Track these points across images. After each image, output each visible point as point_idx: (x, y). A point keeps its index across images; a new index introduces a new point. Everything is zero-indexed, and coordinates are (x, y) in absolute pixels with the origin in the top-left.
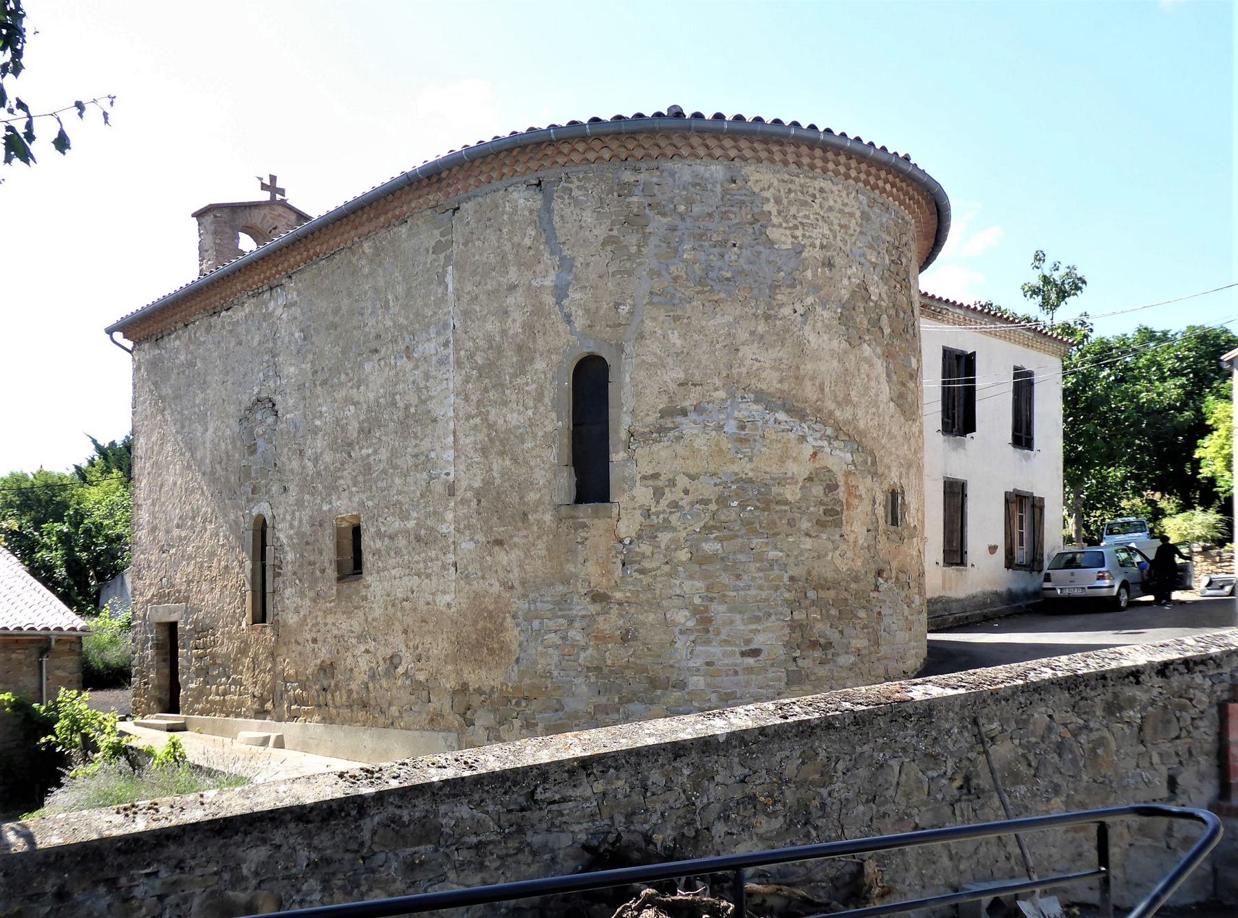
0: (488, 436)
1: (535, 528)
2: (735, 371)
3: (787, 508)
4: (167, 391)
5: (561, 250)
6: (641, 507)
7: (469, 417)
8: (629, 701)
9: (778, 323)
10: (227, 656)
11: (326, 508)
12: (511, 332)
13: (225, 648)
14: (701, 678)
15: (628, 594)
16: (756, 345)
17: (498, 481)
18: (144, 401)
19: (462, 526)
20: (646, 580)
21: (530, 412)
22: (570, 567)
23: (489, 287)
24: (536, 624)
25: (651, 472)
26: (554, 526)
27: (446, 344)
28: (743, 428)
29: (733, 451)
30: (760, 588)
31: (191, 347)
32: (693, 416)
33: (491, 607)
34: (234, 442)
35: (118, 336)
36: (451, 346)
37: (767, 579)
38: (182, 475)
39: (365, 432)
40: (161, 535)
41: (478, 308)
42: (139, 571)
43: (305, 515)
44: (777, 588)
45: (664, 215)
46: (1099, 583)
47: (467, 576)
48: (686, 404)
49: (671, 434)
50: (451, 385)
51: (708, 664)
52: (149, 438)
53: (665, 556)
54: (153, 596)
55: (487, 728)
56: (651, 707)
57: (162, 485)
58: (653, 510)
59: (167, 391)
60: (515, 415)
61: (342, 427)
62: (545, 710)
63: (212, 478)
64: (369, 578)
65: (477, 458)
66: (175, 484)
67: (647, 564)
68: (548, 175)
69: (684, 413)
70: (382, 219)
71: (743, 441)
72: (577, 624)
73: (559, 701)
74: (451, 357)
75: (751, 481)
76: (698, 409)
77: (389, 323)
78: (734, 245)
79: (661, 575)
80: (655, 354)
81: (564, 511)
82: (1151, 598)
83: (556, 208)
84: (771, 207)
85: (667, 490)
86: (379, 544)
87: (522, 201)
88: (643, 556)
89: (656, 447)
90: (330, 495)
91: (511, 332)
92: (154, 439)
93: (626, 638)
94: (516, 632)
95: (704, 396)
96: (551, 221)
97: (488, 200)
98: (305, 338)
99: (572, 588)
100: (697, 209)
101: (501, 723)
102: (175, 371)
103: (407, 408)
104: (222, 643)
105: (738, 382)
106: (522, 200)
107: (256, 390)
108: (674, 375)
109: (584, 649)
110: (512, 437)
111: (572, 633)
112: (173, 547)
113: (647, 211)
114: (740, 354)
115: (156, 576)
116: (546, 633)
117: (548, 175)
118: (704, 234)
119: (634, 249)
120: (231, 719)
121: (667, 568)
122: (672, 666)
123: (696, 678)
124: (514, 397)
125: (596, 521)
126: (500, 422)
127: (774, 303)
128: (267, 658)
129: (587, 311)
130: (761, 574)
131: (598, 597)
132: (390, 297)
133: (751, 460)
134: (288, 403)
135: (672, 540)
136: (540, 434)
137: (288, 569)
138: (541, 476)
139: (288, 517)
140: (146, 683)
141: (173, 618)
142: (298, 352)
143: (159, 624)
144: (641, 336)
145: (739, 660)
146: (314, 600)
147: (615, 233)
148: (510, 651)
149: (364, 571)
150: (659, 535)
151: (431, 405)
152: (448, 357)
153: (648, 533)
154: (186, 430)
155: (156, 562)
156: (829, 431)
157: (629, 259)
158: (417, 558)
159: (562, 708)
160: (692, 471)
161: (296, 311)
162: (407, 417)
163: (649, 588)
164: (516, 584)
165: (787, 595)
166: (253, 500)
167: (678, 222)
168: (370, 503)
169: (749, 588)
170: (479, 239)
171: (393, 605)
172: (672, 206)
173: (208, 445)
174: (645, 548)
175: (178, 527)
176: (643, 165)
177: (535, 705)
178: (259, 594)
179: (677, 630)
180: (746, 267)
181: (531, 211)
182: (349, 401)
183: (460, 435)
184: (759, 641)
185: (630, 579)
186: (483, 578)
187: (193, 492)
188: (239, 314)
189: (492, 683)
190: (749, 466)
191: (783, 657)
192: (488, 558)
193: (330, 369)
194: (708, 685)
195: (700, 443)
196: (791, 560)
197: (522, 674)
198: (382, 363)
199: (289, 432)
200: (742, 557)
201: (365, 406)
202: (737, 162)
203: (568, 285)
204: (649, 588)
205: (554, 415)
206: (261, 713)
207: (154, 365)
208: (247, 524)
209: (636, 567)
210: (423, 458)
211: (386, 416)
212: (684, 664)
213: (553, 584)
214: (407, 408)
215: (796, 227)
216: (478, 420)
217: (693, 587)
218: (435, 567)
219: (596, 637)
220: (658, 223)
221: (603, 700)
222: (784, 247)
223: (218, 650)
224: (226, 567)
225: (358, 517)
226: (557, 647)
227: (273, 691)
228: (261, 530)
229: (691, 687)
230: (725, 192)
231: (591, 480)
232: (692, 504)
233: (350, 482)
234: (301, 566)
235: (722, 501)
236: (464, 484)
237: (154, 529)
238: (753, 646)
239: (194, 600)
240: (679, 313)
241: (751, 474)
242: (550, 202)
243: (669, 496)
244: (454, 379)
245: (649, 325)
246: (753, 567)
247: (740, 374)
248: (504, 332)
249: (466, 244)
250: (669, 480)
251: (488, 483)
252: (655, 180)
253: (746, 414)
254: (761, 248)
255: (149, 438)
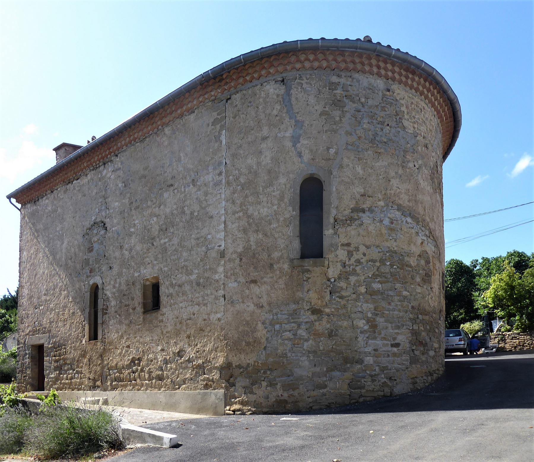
0: (248, 222)
1: (278, 272)
2: (388, 192)
3: (411, 269)
4: (40, 226)
5: (296, 117)
6: (341, 261)
7: (234, 213)
8: (332, 370)
9: (408, 170)
10: (74, 359)
11: (136, 275)
12: (263, 163)
13: (72, 354)
14: (371, 358)
15: (333, 310)
16: (398, 180)
17: (254, 247)
18: (27, 233)
19: (229, 274)
20: (343, 302)
21: (275, 207)
22: (299, 294)
23: (249, 139)
24: (277, 327)
25: (346, 242)
26: (289, 271)
27: (220, 174)
28: (392, 223)
29: (387, 235)
30: (399, 311)
31: (55, 202)
32: (368, 213)
33: (248, 319)
34: (79, 247)
35: (13, 200)
36: (224, 174)
37: (402, 306)
38: (48, 268)
39: (163, 230)
40: (35, 300)
41: (242, 152)
42: (22, 320)
43: (123, 280)
44: (406, 312)
45: (354, 102)
46: (460, 343)
47: (232, 302)
48: (364, 206)
49: (356, 222)
50: (223, 196)
51: (375, 350)
52: (29, 252)
53: (353, 289)
54: (30, 331)
55: (244, 387)
56: (345, 374)
57: (36, 275)
58: (347, 263)
59: (40, 226)
60: (266, 209)
61: (148, 230)
62: (282, 376)
63: (66, 267)
64: (164, 309)
65: (240, 235)
66: (44, 273)
67: (344, 293)
68: (289, 75)
69: (363, 211)
70: (179, 111)
71: (392, 230)
72: (303, 327)
73: (290, 370)
74: (224, 181)
75: (395, 252)
76: (371, 210)
77: (181, 169)
78: (388, 125)
79: (351, 300)
80: (349, 177)
81: (296, 262)
82: (462, 354)
83: (293, 93)
84: (404, 109)
85: (354, 253)
86: (171, 290)
87: (272, 90)
88: (342, 289)
89: (349, 228)
90: (139, 267)
91: (263, 163)
92: (32, 252)
93: (331, 334)
94: (264, 332)
95: (373, 203)
96: (290, 100)
97: (250, 92)
98: (125, 186)
99: (300, 306)
100: (370, 102)
101: (253, 384)
102: (45, 216)
103: (192, 213)
104: (71, 352)
105: (390, 198)
106: (272, 89)
107: (94, 218)
108: (358, 190)
109: (307, 340)
110: (263, 222)
111: (300, 332)
112: (42, 305)
113: (345, 99)
114: (391, 183)
115: (31, 321)
116: (283, 332)
117: (289, 75)
118: (374, 116)
119: (338, 119)
120: (75, 392)
121: (354, 296)
122: (356, 351)
123: (368, 358)
124: (265, 199)
125: (315, 268)
126: (256, 213)
127: (406, 160)
128: (98, 358)
129: (311, 151)
130: (400, 303)
131: (315, 311)
132: (182, 155)
133: (395, 241)
134: (115, 224)
135: (358, 281)
136: (282, 219)
137: (111, 310)
138: (281, 243)
139: (112, 283)
140: (24, 377)
141: (41, 342)
142: (121, 194)
143: (33, 346)
144: (341, 167)
145: (390, 349)
146: (129, 325)
147: (327, 109)
148: (260, 343)
149: (161, 307)
150: (350, 277)
151: (208, 209)
152: (221, 181)
153: (344, 276)
154: (51, 244)
155: (32, 314)
156: (427, 233)
157: (335, 124)
158: (197, 295)
159: (292, 375)
160: (368, 243)
161: (120, 173)
162: (192, 218)
163: (345, 307)
164: (265, 304)
165: (411, 315)
166: (90, 276)
167: (360, 107)
168: (166, 269)
169: (394, 310)
170: (243, 114)
171: (181, 323)
172: (358, 98)
173: (64, 251)
174: (343, 284)
175: (45, 295)
176: (343, 74)
177: (275, 373)
178: (93, 326)
179: (359, 331)
180: (393, 138)
181: (278, 96)
182: (152, 215)
183: (229, 223)
184: (400, 339)
185: (334, 302)
186: (243, 302)
187: (54, 275)
188: (84, 180)
189: (248, 361)
190: (395, 244)
191: (408, 349)
192: (247, 291)
193: (141, 200)
194: (375, 362)
195: (371, 228)
196: (412, 297)
197: (268, 356)
198: (176, 191)
199: (114, 237)
200: (391, 293)
201: (163, 216)
202: (390, 81)
203: (300, 136)
204: (345, 307)
205: (290, 209)
206: (94, 387)
207: (32, 215)
208: (86, 289)
209: (338, 294)
210: (202, 239)
211: (178, 220)
212: (362, 350)
213: (288, 304)
214: (192, 213)
215: (414, 123)
216: (241, 214)
217: (368, 307)
218: (211, 299)
219: (314, 334)
220: (350, 106)
221: (317, 369)
222: (410, 131)
223: (67, 356)
224: (73, 313)
225: (157, 278)
226: (290, 339)
227: (101, 375)
228: (95, 291)
229: (366, 363)
230: (384, 95)
231: (312, 248)
232: (368, 261)
233: (153, 259)
234: (120, 308)
235: (382, 261)
236: (231, 250)
237: (31, 297)
238: (396, 342)
239: (53, 332)
240: (361, 156)
241: (395, 249)
242: (290, 90)
243: (356, 256)
244: (224, 193)
245: (346, 160)
246: (396, 298)
247: (391, 194)
248: (259, 164)
249: (234, 117)
250: (355, 248)
251: (247, 249)
252: (349, 83)
253: (394, 216)
254: (399, 130)
255: (29, 252)
